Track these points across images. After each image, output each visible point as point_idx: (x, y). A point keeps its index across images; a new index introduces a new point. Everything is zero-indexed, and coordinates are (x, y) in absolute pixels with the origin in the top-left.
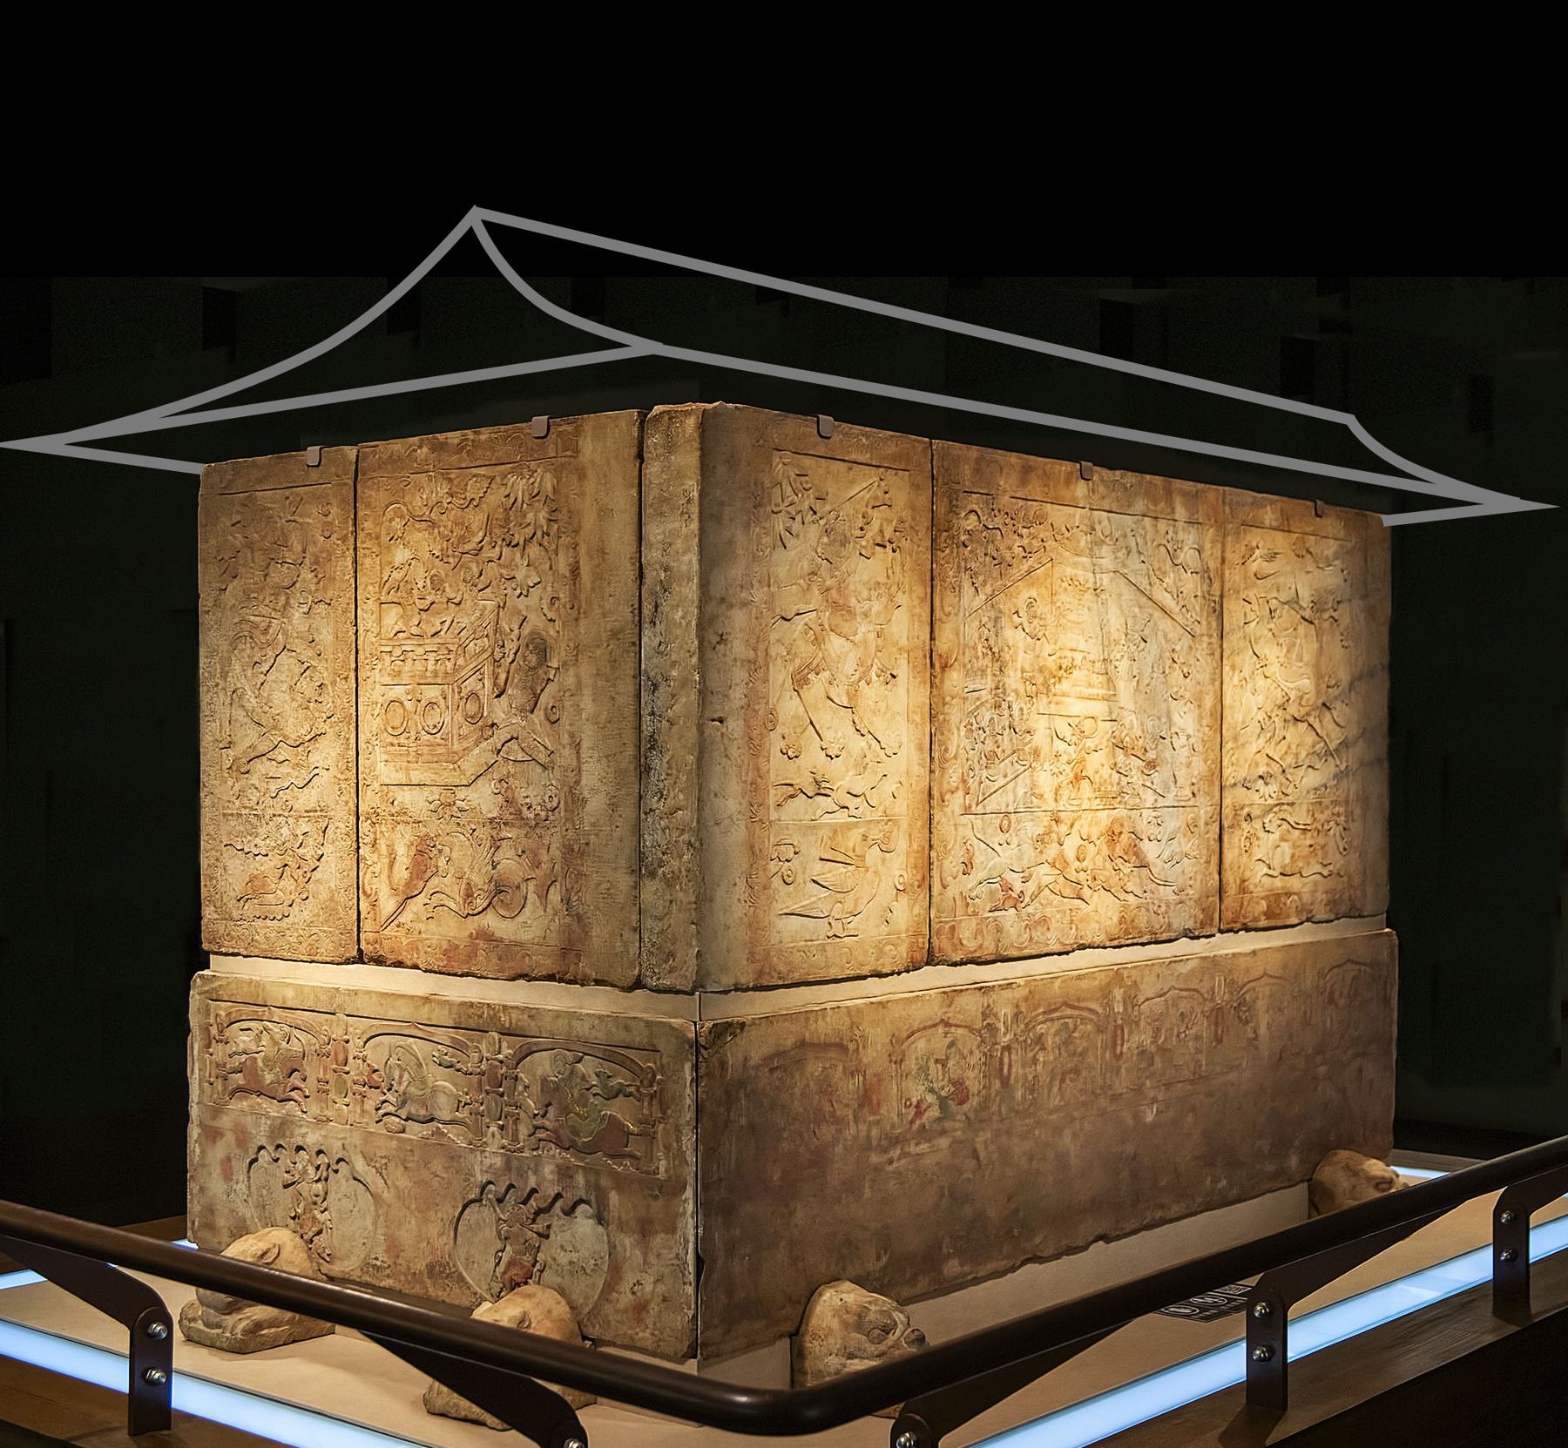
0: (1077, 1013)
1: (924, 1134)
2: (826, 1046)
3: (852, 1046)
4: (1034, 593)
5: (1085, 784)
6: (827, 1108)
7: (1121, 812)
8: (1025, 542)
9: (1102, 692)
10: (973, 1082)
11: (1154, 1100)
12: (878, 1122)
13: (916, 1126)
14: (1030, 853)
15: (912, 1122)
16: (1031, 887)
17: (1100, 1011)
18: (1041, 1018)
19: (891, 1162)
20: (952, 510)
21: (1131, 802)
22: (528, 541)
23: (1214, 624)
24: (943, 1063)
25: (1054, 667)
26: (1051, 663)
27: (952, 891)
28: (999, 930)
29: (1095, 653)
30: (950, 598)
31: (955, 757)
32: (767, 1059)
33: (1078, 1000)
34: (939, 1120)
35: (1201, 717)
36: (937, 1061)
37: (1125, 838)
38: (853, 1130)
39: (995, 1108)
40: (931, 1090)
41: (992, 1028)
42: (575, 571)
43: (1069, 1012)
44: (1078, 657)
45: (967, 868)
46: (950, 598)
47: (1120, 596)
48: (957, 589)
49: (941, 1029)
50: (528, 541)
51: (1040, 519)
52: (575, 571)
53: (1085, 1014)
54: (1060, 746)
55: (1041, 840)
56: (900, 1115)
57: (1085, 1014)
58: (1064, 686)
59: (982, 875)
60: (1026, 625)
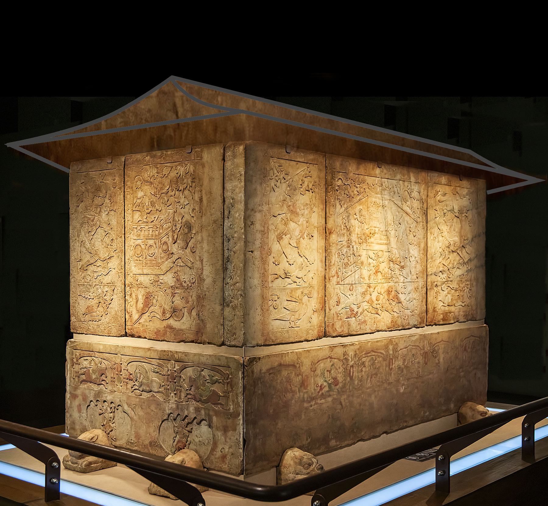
0: (376, 354)
1: (323, 396)
2: (289, 366)
3: (298, 366)
4: (361, 207)
5: (379, 274)
6: (289, 387)
7: (392, 284)
8: (358, 189)
9: (385, 242)
10: (340, 378)
11: (403, 385)
12: (307, 392)
13: (320, 393)
14: (360, 298)
15: (319, 392)
16: (360, 310)
17: (385, 353)
18: (364, 356)
19: (311, 406)
20: (333, 178)
21: (395, 280)
22: (184, 189)
23: (424, 218)
24: (329, 371)
25: (368, 233)
26: (367, 232)
27: (333, 311)
28: (349, 325)
29: (383, 228)
30: (332, 209)
31: (334, 265)
32: (268, 370)
33: (377, 349)
34: (328, 391)
35: (420, 251)
36: (327, 371)
37: (393, 293)
38: (298, 395)
39: (348, 387)
40: (326, 381)
41: (347, 359)
42: (201, 200)
43: (374, 354)
44: (377, 230)
45: (338, 303)
46: (332, 209)
47: (391, 208)
48: (334, 206)
49: (329, 360)
50: (184, 189)
51: (364, 181)
52: (201, 200)
53: (379, 354)
54: (370, 261)
55: (364, 294)
56: (314, 389)
57: (379, 354)
58: (372, 240)
59: (343, 306)
60: (359, 218)
